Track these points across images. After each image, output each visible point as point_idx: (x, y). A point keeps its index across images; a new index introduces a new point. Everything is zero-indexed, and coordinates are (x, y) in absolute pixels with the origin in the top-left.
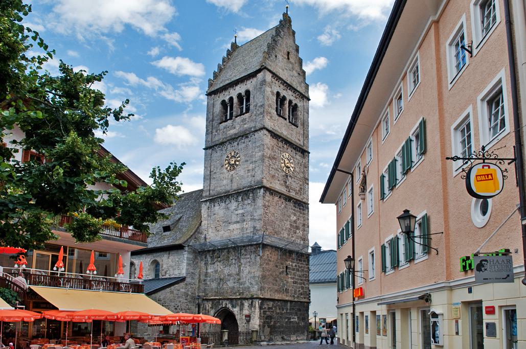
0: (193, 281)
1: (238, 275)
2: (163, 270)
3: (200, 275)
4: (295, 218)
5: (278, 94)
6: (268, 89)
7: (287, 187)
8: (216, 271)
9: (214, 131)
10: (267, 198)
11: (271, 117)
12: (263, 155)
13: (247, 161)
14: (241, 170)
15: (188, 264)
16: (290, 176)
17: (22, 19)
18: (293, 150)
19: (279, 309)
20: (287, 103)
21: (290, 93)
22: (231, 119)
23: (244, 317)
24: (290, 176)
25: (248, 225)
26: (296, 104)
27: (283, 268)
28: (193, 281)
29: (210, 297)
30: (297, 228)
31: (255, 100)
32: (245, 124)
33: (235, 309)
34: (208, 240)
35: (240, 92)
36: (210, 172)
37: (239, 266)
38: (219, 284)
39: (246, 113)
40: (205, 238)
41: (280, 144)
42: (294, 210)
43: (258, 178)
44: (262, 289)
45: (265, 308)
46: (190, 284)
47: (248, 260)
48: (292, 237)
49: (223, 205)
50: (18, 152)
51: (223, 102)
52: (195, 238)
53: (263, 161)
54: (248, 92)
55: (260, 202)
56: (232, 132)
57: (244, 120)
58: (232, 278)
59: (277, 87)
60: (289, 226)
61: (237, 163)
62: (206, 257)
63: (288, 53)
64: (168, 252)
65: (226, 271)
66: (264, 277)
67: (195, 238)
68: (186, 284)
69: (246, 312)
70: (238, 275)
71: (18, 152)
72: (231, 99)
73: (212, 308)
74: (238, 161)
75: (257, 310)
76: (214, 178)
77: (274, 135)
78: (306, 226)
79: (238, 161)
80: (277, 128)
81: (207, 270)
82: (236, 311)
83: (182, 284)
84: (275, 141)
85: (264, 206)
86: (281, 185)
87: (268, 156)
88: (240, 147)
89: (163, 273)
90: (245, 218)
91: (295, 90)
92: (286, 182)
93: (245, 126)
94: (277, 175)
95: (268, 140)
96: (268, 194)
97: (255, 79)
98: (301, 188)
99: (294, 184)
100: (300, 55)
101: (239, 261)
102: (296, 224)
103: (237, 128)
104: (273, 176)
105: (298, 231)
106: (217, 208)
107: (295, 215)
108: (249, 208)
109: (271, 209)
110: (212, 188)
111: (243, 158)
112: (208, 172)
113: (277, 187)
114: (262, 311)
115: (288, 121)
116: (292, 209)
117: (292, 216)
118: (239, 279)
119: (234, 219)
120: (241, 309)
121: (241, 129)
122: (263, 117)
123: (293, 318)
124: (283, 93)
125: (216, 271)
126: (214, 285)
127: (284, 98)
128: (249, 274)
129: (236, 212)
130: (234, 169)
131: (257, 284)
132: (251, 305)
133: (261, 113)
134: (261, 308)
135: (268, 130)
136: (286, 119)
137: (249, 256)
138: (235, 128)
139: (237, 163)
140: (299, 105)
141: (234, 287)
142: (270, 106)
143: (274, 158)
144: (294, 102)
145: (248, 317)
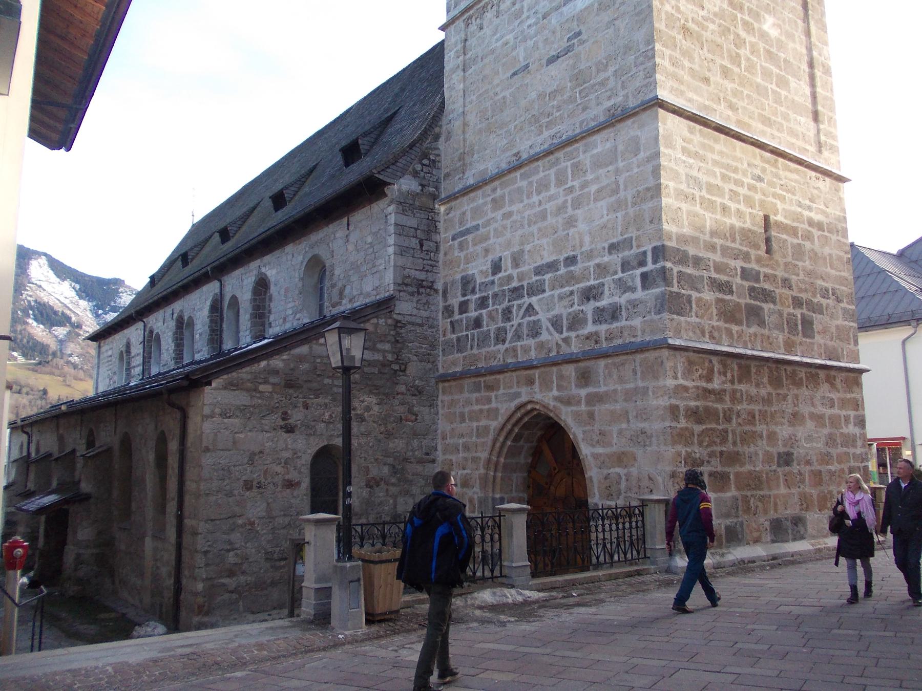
15: (402, 251)
89: (335, 291)
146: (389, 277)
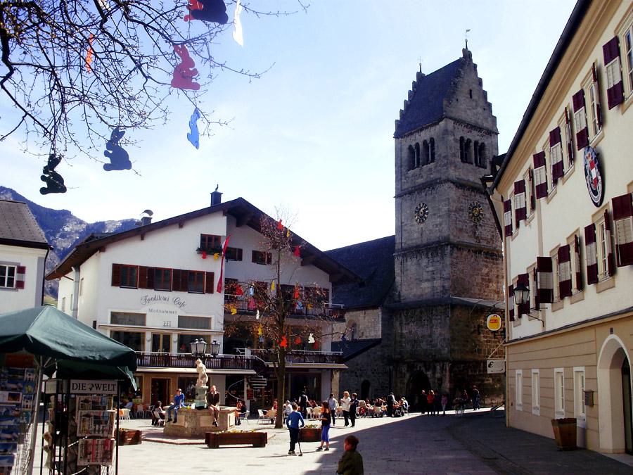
0: (389, 343)
1: (430, 336)
2: (359, 331)
3: (395, 336)
4: (487, 270)
5: (462, 138)
6: (451, 138)
7: (477, 238)
8: (410, 332)
9: (403, 178)
10: (455, 255)
11: (455, 167)
12: (449, 210)
13: (435, 215)
14: (430, 223)
16: (480, 225)
17: (253, 261)
18: (482, 196)
19: (471, 371)
20: (472, 144)
21: (475, 133)
22: (418, 167)
23: (436, 381)
24: (480, 225)
25: (437, 283)
26: (483, 144)
27: (475, 327)
28: (389, 343)
29: (47, 315)
30: (490, 281)
31: (440, 150)
32: (431, 174)
33: (428, 373)
34: (402, 298)
35: (425, 138)
36: (402, 223)
37: (431, 327)
38: (413, 346)
39: (431, 162)
40: (399, 296)
41: (467, 193)
42: (486, 262)
43: (446, 234)
44: (452, 351)
45: (456, 371)
46: (386, 346)
47: (439, 321)
48: (484, 292)
49: (415, 260)
50: (240, 259)
51: (410, 147)
52: (390, 296)
53: (449, 216)
54: (432, 140)
55: (448, 260)
56: (420, 181)
57: (430, 169)
58: (425, 340)
59: (462, 132)
60: (480, 281)
61: (426, 216)
62: (400, 317)
63: (471, 91)
64: (364, 312)
65: (420, 332)
66: (453, 339)
67: (390, 296)
68: (382, 347)
69: (438, 375)
70: (430, 336)
71: (240, 259)
72: (417, 145)
73: (408, 371)
74: (427, 214)
75: (448, 374)
76: (405, 230)
77: (460, 185)
78: (500, 277)
79: (427, 214)
80: (463, 177)
81: (402, 330)
82: (429, 373)
83: (378, 347)
84: (461, 191)
85: (452, 264)
86: (470, 236)
87: (454, 209)
88: (428, 198)
90: (435, 276)
91: (480, 129)
92: (475, 233)
93: (432, 176)
94: (464, 227)
95: (454, 192)
96: (455, 250)
97: (438, 126)
98: (493, 236)
99: (484, 232)
100: (484, 88)
101: (431, 322)
102: (488, 276)
103: (425, 177)
104: (461, 230)
105: (491, 285)
106: (409, 263)
107: (487, 266)
108: (439, 266)
109: (460, 266)
110: (404, 241)
111: (430, 211)
112: (400, 224)
113: (466, 241)
114: (452, 374)
115: (474, 165)
116: (483, 261)
117: (484, 268)
118: (431, 341)
119: (425, 276)
120: (434, 373)
121: (428, 179)
122: (447, 169)
123: (487, 380)
124: (467, 136)
125: (410, 332)
126: (408, 347)
127: (469, 141)
128: (438, 333)
129: (427, 270)
130: (423, 221)
131: (447, 346)
132: (442, 369)
133: (445, 165)
134: (451, 371)
135: (453, 182)
136: (472, 164)
137: (439, 317)
138: (422, 177)
139: (426, 216)
140: (486, 143)
141: (426, 350)
142: (454, 155)
143: (461, 210)
144: (480, 142)
145: (440, 380)
146: (380, 333)
